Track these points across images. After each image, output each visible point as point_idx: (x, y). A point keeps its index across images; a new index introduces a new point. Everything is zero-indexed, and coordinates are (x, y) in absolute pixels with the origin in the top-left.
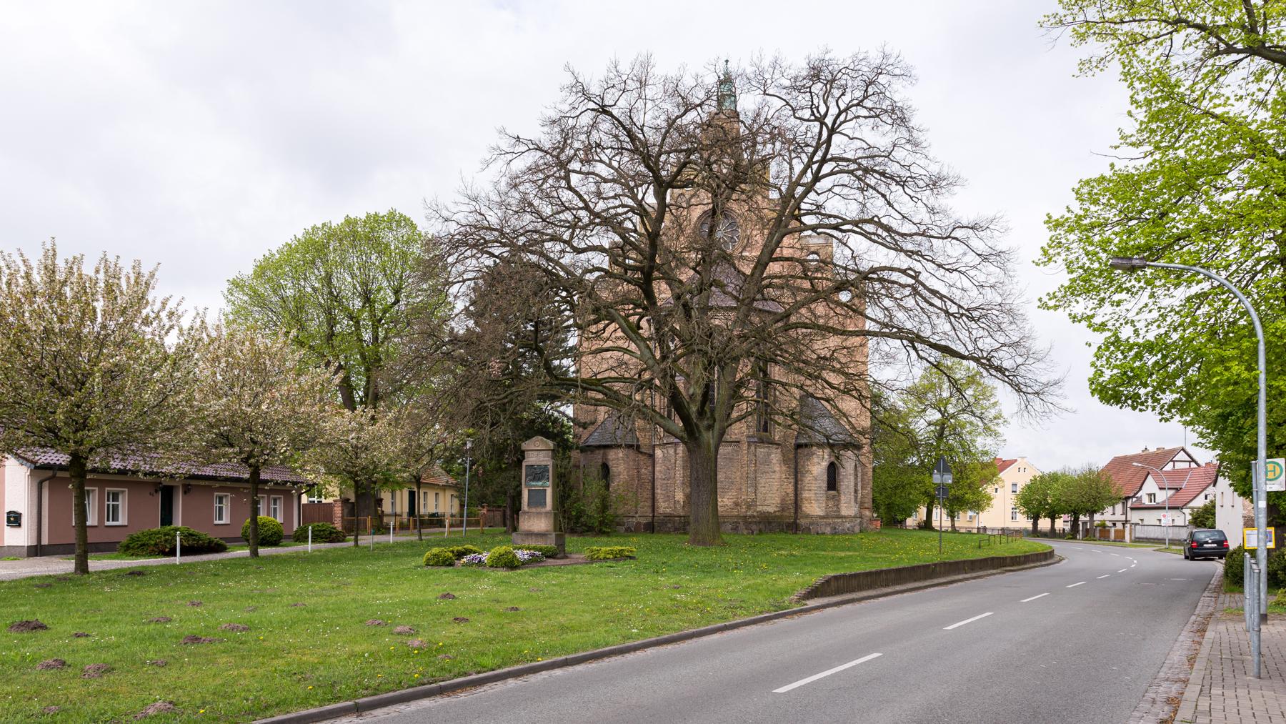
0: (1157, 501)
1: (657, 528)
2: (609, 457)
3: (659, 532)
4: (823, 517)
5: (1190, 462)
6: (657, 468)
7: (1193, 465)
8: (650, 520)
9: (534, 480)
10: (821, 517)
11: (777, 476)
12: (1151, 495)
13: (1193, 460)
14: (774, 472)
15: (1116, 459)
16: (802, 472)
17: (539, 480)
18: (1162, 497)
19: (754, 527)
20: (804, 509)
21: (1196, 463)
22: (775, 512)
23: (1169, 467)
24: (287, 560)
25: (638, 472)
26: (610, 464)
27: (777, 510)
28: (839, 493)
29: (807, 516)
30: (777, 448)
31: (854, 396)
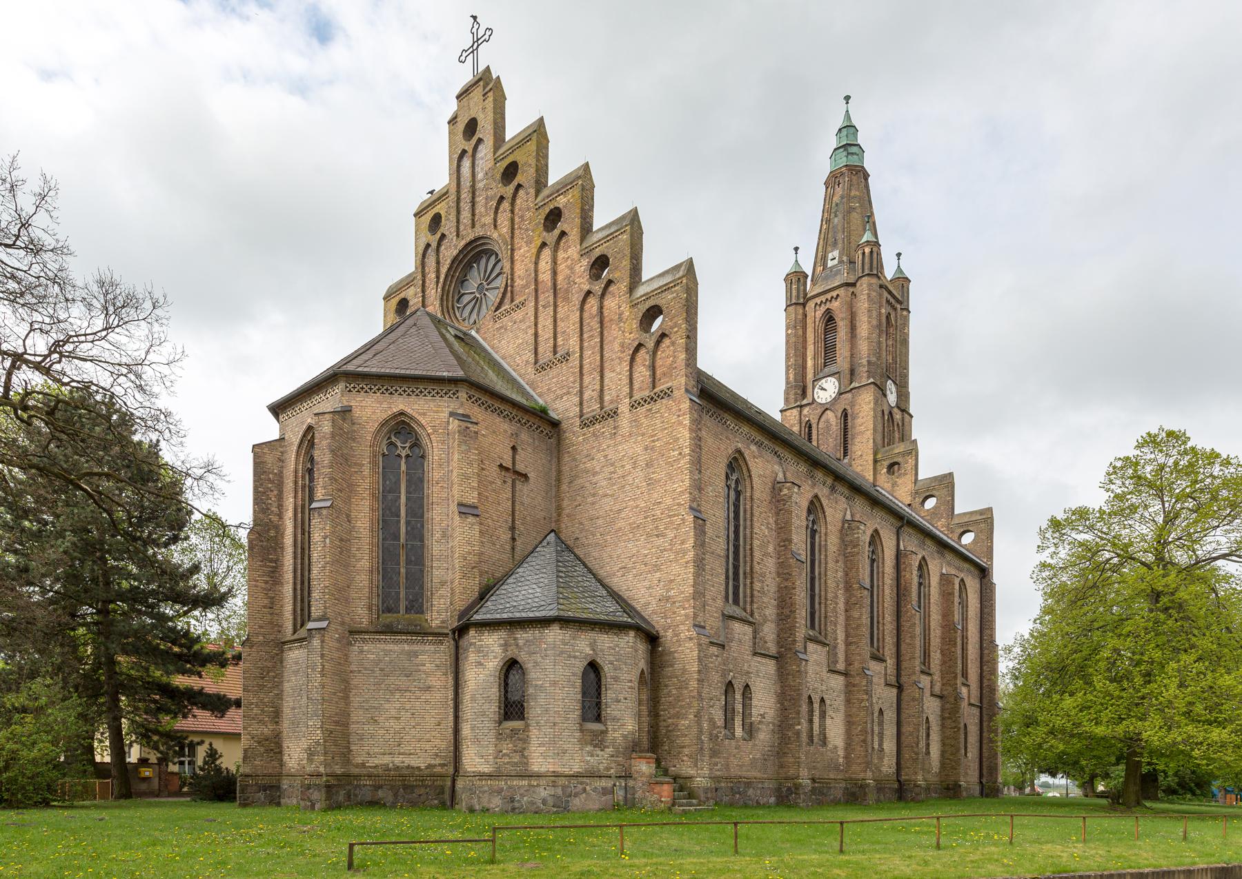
4: (490, 776)
10: (482, 776)
14: (428, 689)
22: (429, 766)
24: (1164, 811)
27: (438, 761)
28: (527, 726)
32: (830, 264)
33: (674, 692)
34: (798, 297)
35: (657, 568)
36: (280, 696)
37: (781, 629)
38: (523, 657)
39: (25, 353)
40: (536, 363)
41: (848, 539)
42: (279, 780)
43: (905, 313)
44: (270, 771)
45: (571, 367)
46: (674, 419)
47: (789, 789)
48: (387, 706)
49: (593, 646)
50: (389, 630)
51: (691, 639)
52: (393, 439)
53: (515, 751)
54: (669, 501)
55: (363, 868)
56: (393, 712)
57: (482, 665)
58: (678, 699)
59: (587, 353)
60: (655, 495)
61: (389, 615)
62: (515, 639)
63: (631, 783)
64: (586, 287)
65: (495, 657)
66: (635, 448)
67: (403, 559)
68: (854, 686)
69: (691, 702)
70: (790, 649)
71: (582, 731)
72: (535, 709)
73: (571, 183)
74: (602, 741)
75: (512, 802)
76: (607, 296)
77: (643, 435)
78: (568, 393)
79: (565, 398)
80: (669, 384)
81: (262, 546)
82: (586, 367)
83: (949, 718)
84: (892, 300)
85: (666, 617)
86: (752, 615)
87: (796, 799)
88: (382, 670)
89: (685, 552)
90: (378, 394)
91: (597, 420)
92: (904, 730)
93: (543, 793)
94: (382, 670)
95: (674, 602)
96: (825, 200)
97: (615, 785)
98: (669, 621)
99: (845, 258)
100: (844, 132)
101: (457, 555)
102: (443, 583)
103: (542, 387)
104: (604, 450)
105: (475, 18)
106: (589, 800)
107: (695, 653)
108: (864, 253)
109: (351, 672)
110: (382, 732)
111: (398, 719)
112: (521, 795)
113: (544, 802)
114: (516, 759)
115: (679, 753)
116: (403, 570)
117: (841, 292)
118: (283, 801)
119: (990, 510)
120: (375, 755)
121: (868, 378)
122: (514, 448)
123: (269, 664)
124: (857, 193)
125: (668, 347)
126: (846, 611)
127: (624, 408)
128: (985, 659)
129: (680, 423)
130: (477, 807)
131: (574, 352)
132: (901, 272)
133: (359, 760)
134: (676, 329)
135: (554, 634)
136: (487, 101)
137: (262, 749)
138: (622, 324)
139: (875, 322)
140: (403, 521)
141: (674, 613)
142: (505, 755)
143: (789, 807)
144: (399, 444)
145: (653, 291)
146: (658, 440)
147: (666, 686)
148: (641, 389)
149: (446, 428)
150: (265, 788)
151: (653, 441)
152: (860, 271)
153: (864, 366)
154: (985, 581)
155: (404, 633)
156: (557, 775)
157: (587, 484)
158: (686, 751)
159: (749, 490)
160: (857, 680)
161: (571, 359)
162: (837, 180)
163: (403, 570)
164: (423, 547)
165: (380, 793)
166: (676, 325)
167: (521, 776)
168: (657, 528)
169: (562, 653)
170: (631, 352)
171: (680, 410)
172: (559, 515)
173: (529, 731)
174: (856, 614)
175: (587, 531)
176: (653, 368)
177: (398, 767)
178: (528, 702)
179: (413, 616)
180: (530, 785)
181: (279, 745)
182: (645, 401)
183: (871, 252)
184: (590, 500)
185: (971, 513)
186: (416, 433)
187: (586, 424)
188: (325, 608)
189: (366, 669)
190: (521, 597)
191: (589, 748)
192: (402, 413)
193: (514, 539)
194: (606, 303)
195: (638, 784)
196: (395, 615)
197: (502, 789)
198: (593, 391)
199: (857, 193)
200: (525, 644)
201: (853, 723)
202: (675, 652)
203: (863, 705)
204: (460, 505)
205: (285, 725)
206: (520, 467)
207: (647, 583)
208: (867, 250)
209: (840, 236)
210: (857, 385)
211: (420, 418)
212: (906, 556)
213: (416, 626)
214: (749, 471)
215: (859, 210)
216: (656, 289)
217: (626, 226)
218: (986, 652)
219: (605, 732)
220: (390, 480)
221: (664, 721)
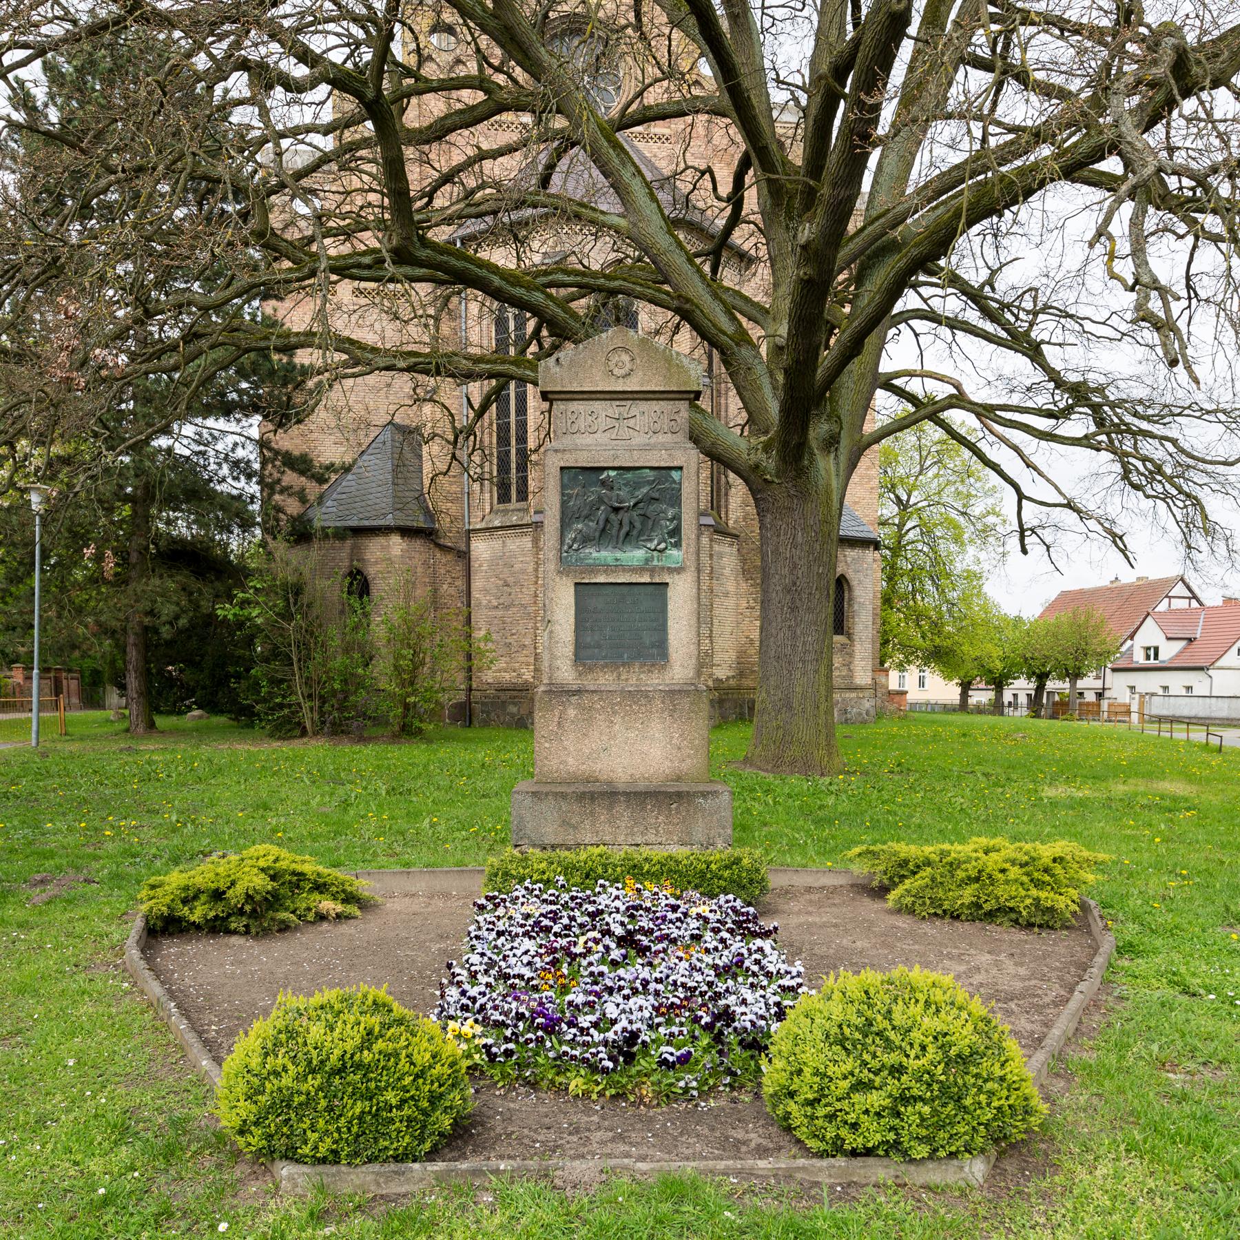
0: (1161, 657)
1: (479, 715)
2: (368, 556)
3: (486, 724)
5: (1190, 598)
6: (477, 583)
7: (1194, 604)
8: (462, 697)
9: (603, 536)
11: (730, 602)
12: (1148, 648)
13: (1195, 597)
14: (726, 595)
15: (1064, 594)
17: (629, 538)
18: (1169, 651)
21: (1198, 601)
22: (728, 678)
23: (1163, 606)
25: (436, 590)
26: (371, 571)
27: (730, 674)
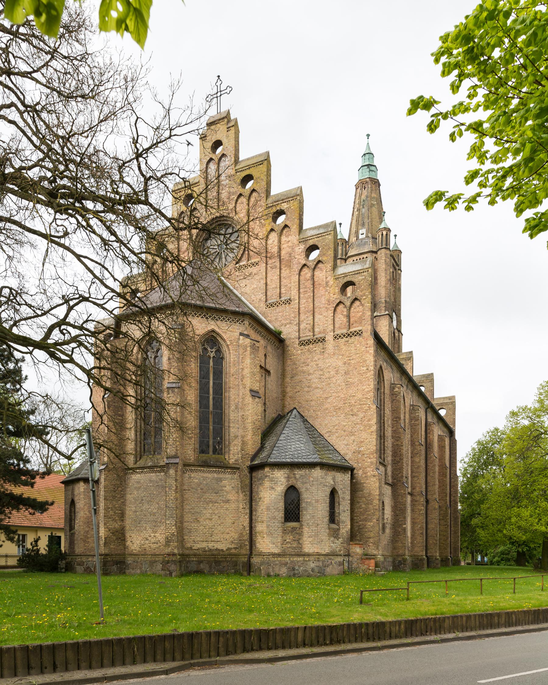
4: (279, 555)
10: (274, 555)
11: (233, 506)
14: (228, 501)
16: (255, 500)
19: (173, 567)
20: (258, 545)
22: (229, 549)
27: (233, 546)
28: (302, 525)
29: (261, 554)
30: (235, 473)
31: (37, 81)
32: (361, 237)
33: (363, 506)
34: (342, 254)
35: (352, 434)
36: (124, 503)
37: (395, 469)
38: (299, 485)
39: (90, 297)
40: (266, 301)
41: (413, 415)
42: (124, 558)
43: (399, 272)
44: (119, 552)
45: (293, 308)
46: (363, 349)
47: (400, 561)
48: (204, 512)
49: (334, 479)
50: (206, 465)
51: (374, 476)
52: (206, 346)
53: (294, 540)
54: (360, 396)
55: (368, 603)
56: (208, 515)
57: (273, 489)
58: (366, 510)
59: (303, 301)
60: (351, 391)
61: (203, 455)
62: (294, 474)
63: (351, 559)
64: (303, 262)
65: (282, 485)
66: (337, 362)
67: (211, 420)
68: (416, 501)
69: (375, 512)
70: (400, 481)
71: (329, 528)
72: (306, 515)
73: (292, 197)
74: (338, 535)
75: (294, 570)
76: (316, 270)
77: (343, 355)
78: (290, 323)
79: (288, 326)
80: (360, 328)
81: (114, 406)
82: (302, 309)
83: (443, 519)
84: (395, 264)
85: (358, 463)
86: (384, 461)
87: (404, 567)
88: (202, 489)
89: (370, 426)
90: (200, 318)
91: (311, 342)
92: (429, 526)
93: (312, 565)
94: (202, 489)
95: (364, 454)
96: (355, 195)
97: (344, 560)
98: (360, 465)
99: (370, 235)
100: (367, 156)
101: (249, 421)
102: (236, 437)
103: (271, 317)
104: (316, 361)
105: (219, 76)
106: (333, 569)
107: (377, 484)
108: (382, 234)
109: (184, 490)
110: (202, 528)
111: (211, 519)
112: (299, 566)
113: (313, 570)
114: (295, 545)
115: (367, 541)
116: (211, 428)
117: (368, 255)
118: (127, 571)
119: (454, 397)
120: (198, 542)
121: (385, 310)
122: (265, 355)
123: (118, 483)
124: (375, 196)
125: (358, 306)
126: (412, 457)
127: (330, 337)
128: (452, 484)
129: (367, 352)
130: (272, 574)
131: (294, 300)
132: (397, 247)
133: (188, 545)
134: (364, 297)
135: (317, 472)
136: (229, 132)
137: (115, 538)
138: (328, 288)
139: (388, 277)
140: (211, 397)
141: (364, 460)
142: (287, 543)
143: (58, 572)
144: (209, 349)
145: (349, 273)
146: (353, 359)
147: (358, 502)
148: (340, 328)
149: (237, 342)
150: (117, 563)
151: (350, 360)
152: (380, 245)
153: (383, 303)
154: (452, 439)
155: (215, 467)
156: (319, 554)
157: (304, 380)
158: (371, 540)
159: (382, 388)
160: (418, 498)
161: (292, 303)
162: (364, 185)
163: (211, 428)
164: (222, 414)
165: (202, 566)
166: (364, 295)
167: (299, 555)
168: (352, 410)
169: (321, 483)
170: (334, 306)
171: (367, 344)
172: (284, 396)
173: (303, 529)
174: (417, 460)
175: (303, 407)
176: (348, 317)
177: (211, 550)
178: (302, 511)
179: (217, 456)
180: (304, 560)
181: (123, 535)
182: (344, 336)
183: (387, 234)
184: (306, 389)
185: (444, 398)
186: (219, 343)
187: (302, 344)
188: (177, 450)
189: (192, 488)
190: (293, 449)
191: (332, 539)
192: (213, 331)
193: (265, 410)
194: (316, 273)
195: (354, 560)
196: (206, 455)
197: (287, 563)
198: (307, 324)
199: (375, 196)
200: (300, 478)
201: (416, 523)
202: (364, 483)
203: (421, 512)
204: (251, 391)
205: (128, 522)
206: (268, 367)
207: (345, 442)
208: (385, 233)
209: (366, 221)
210: (379, 314)
211: (223, 335)
212: (430, 425)
213: (220, 462)
214: (383, 377)
215: (376, 206)
216: (351, 272)
217: (331, 231)
218: (453, 480)
219: (339, 529)
220: (203, 371)
221: (357, 522)
